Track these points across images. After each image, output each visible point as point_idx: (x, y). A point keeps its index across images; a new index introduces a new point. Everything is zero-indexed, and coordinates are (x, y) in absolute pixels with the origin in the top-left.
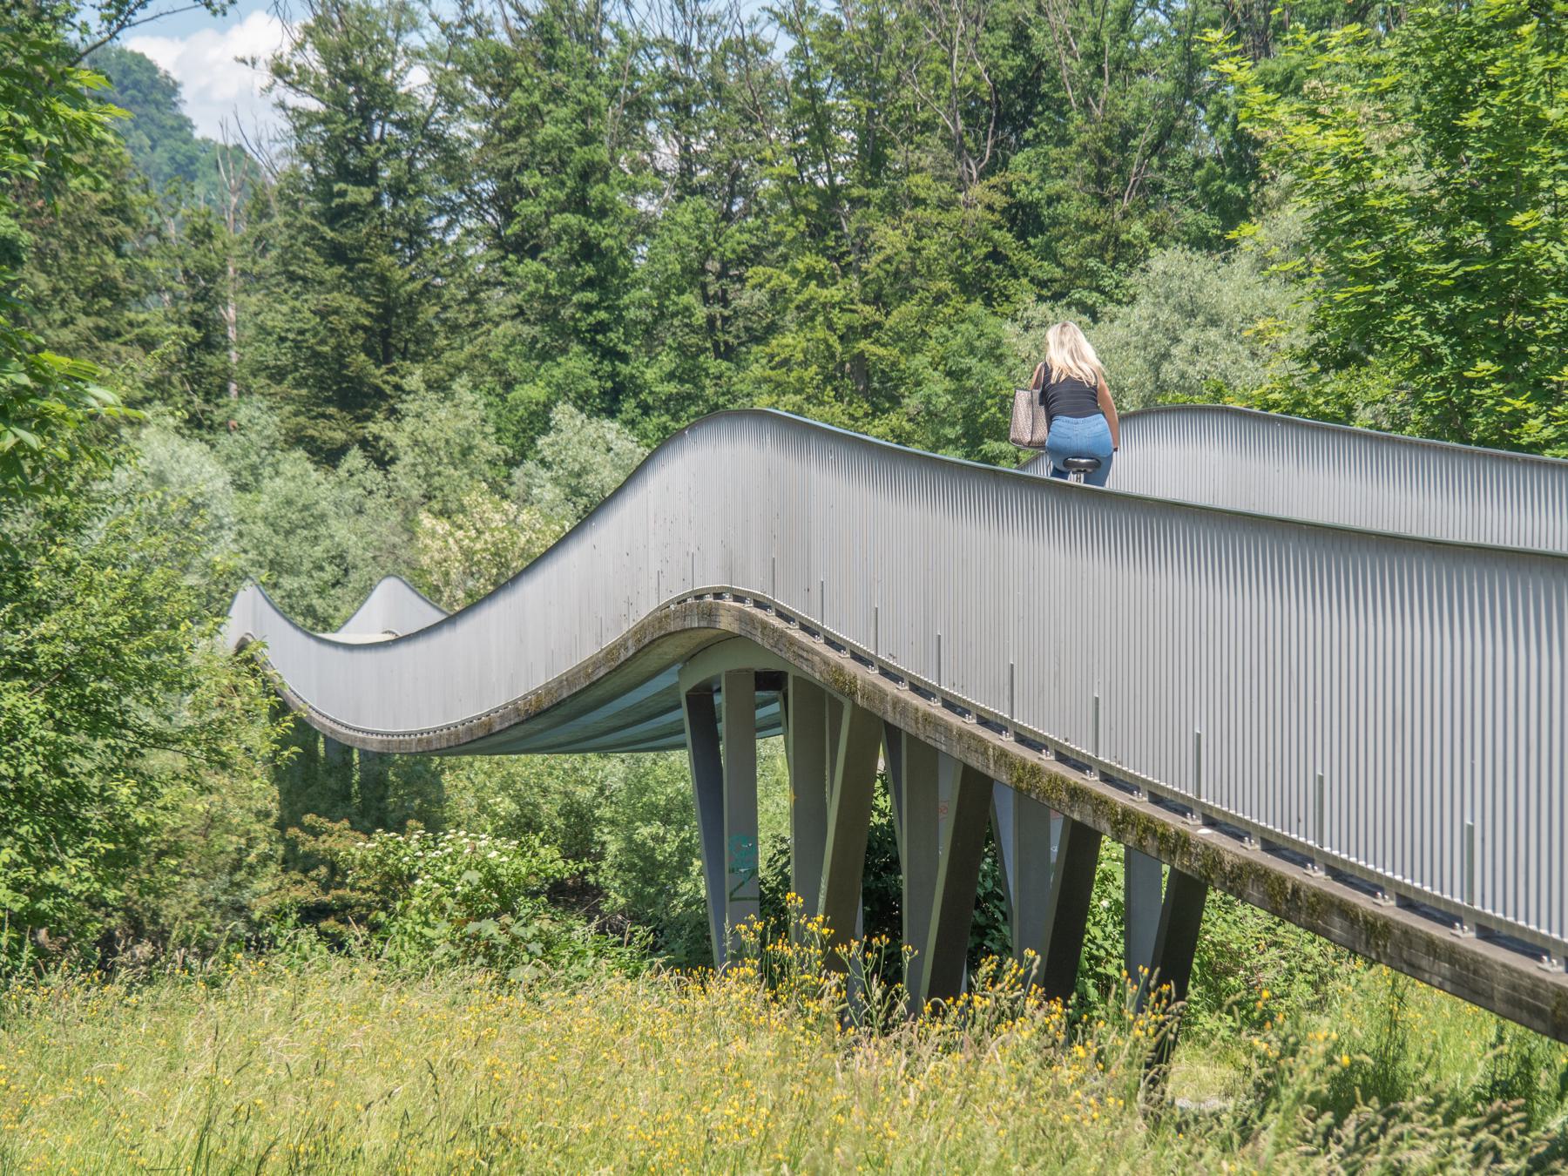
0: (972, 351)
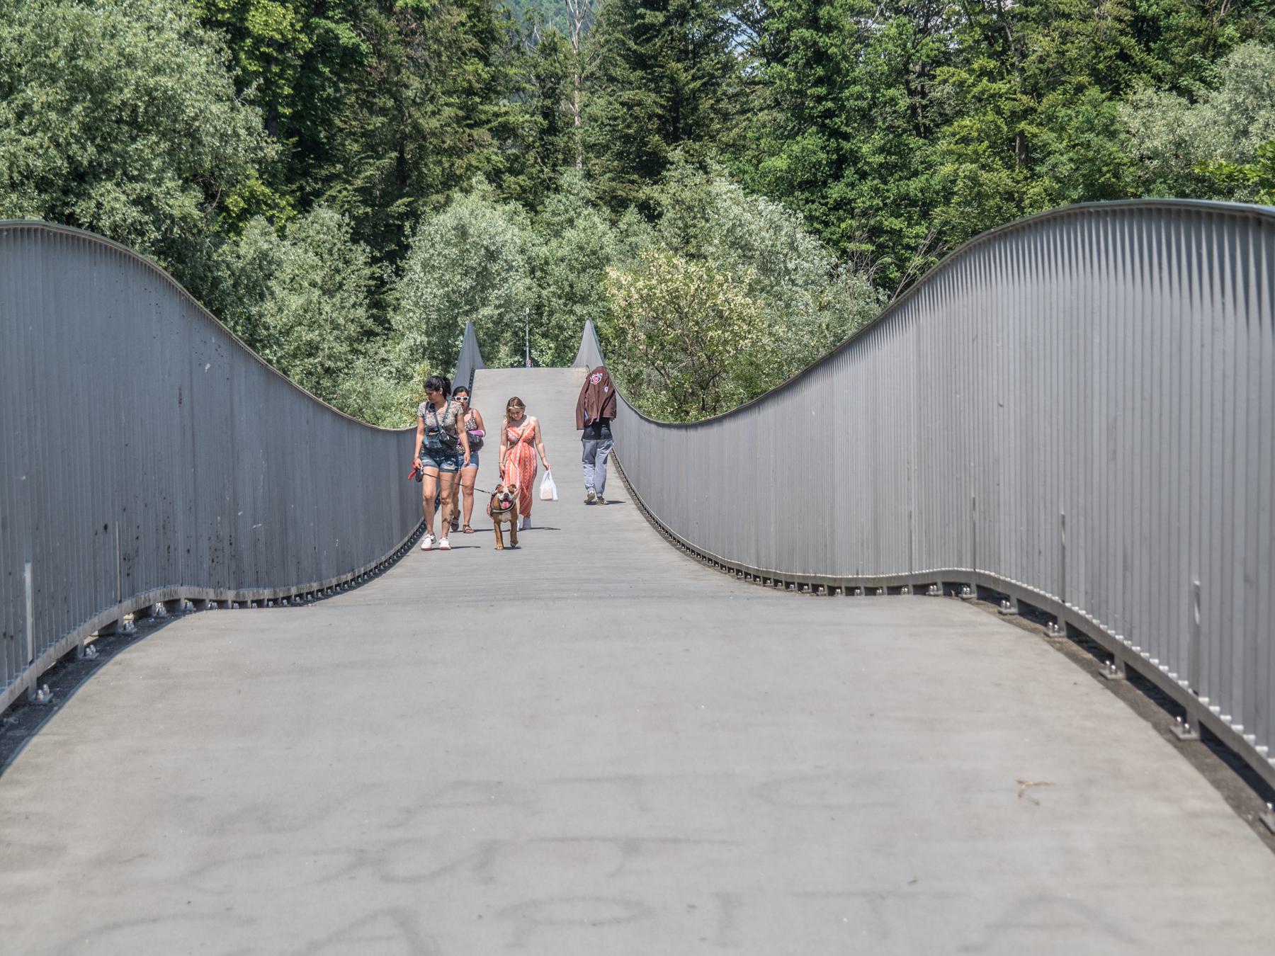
0: (1092, 129)
